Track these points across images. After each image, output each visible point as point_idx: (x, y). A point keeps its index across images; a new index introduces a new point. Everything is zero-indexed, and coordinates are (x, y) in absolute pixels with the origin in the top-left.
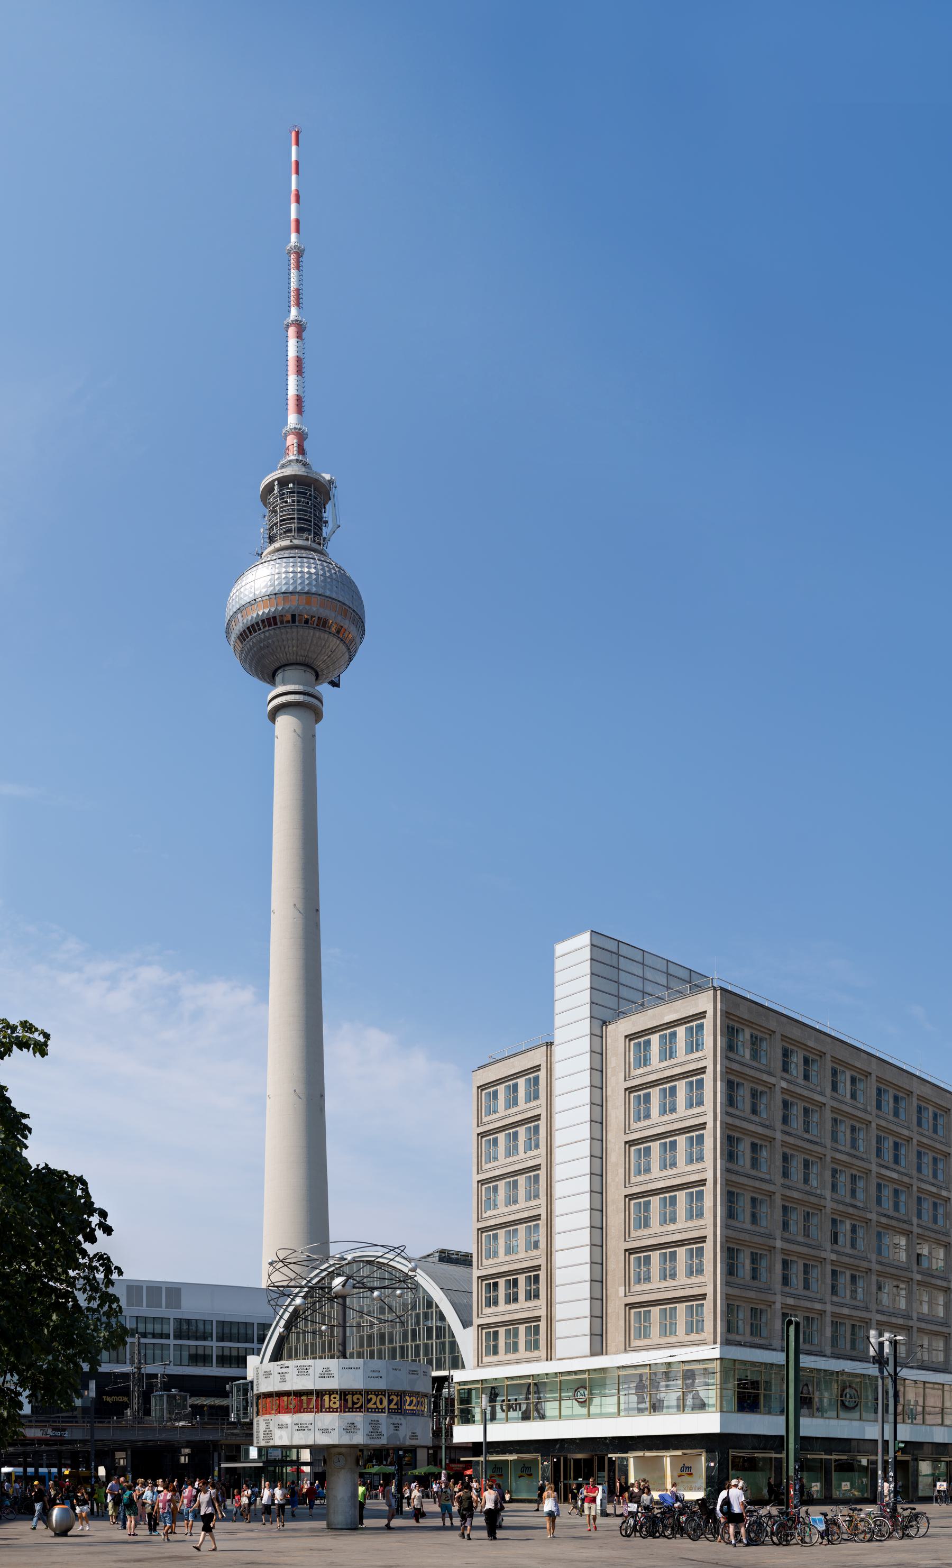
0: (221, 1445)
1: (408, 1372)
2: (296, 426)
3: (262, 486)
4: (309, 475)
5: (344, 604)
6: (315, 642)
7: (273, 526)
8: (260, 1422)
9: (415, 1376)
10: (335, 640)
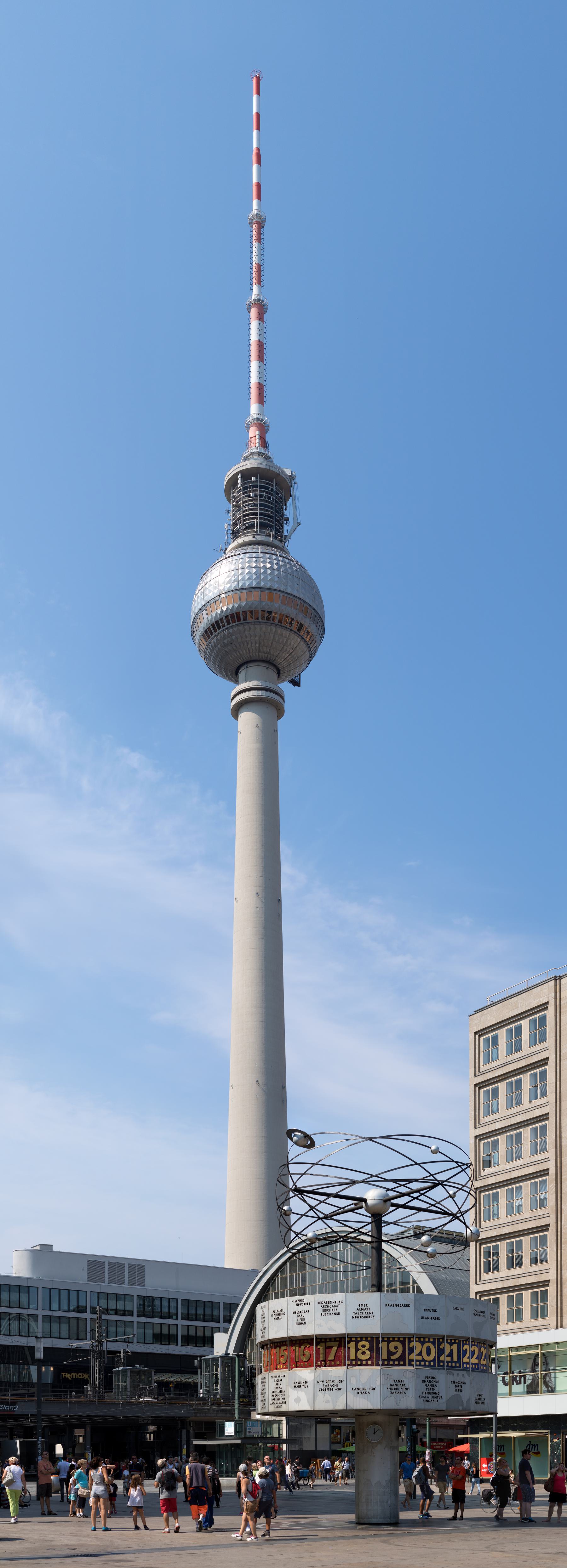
0: (190, 1422)
1: (473, 1312)
2: (258, 417)
3: (226, 480)
4: (271, 469)
5: (305, 602)
6: (277, 639)
7: (236, 521)
8: (267, 1380)
9: (482, 1318)
10: (296, 637)
